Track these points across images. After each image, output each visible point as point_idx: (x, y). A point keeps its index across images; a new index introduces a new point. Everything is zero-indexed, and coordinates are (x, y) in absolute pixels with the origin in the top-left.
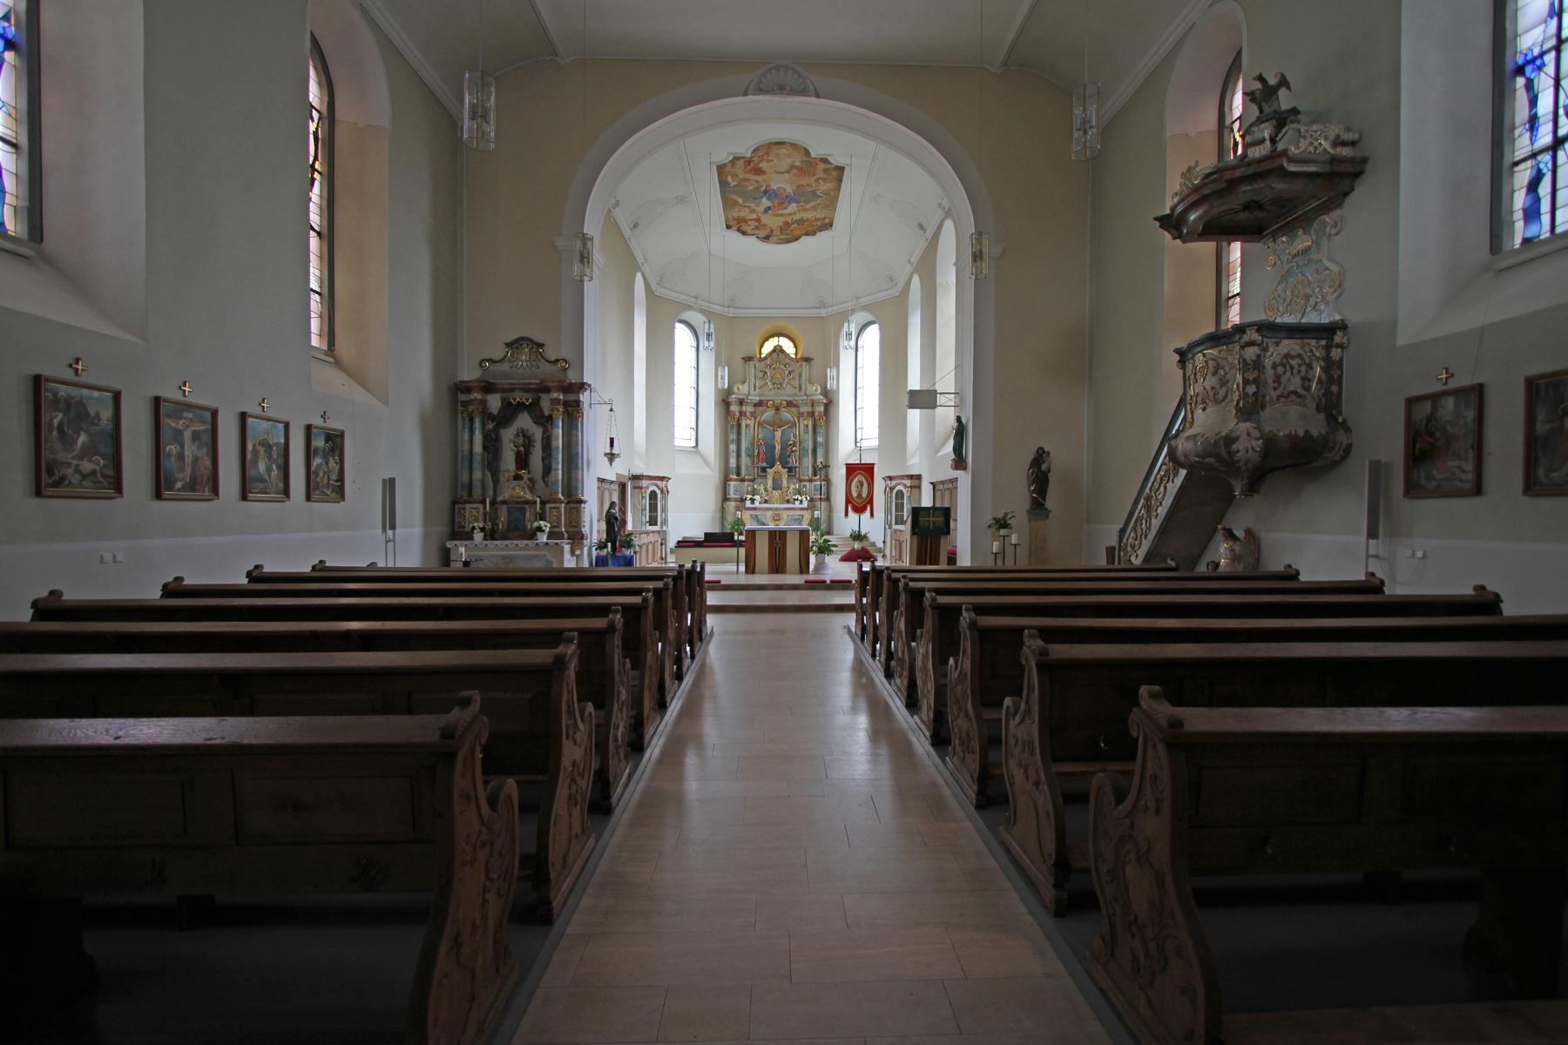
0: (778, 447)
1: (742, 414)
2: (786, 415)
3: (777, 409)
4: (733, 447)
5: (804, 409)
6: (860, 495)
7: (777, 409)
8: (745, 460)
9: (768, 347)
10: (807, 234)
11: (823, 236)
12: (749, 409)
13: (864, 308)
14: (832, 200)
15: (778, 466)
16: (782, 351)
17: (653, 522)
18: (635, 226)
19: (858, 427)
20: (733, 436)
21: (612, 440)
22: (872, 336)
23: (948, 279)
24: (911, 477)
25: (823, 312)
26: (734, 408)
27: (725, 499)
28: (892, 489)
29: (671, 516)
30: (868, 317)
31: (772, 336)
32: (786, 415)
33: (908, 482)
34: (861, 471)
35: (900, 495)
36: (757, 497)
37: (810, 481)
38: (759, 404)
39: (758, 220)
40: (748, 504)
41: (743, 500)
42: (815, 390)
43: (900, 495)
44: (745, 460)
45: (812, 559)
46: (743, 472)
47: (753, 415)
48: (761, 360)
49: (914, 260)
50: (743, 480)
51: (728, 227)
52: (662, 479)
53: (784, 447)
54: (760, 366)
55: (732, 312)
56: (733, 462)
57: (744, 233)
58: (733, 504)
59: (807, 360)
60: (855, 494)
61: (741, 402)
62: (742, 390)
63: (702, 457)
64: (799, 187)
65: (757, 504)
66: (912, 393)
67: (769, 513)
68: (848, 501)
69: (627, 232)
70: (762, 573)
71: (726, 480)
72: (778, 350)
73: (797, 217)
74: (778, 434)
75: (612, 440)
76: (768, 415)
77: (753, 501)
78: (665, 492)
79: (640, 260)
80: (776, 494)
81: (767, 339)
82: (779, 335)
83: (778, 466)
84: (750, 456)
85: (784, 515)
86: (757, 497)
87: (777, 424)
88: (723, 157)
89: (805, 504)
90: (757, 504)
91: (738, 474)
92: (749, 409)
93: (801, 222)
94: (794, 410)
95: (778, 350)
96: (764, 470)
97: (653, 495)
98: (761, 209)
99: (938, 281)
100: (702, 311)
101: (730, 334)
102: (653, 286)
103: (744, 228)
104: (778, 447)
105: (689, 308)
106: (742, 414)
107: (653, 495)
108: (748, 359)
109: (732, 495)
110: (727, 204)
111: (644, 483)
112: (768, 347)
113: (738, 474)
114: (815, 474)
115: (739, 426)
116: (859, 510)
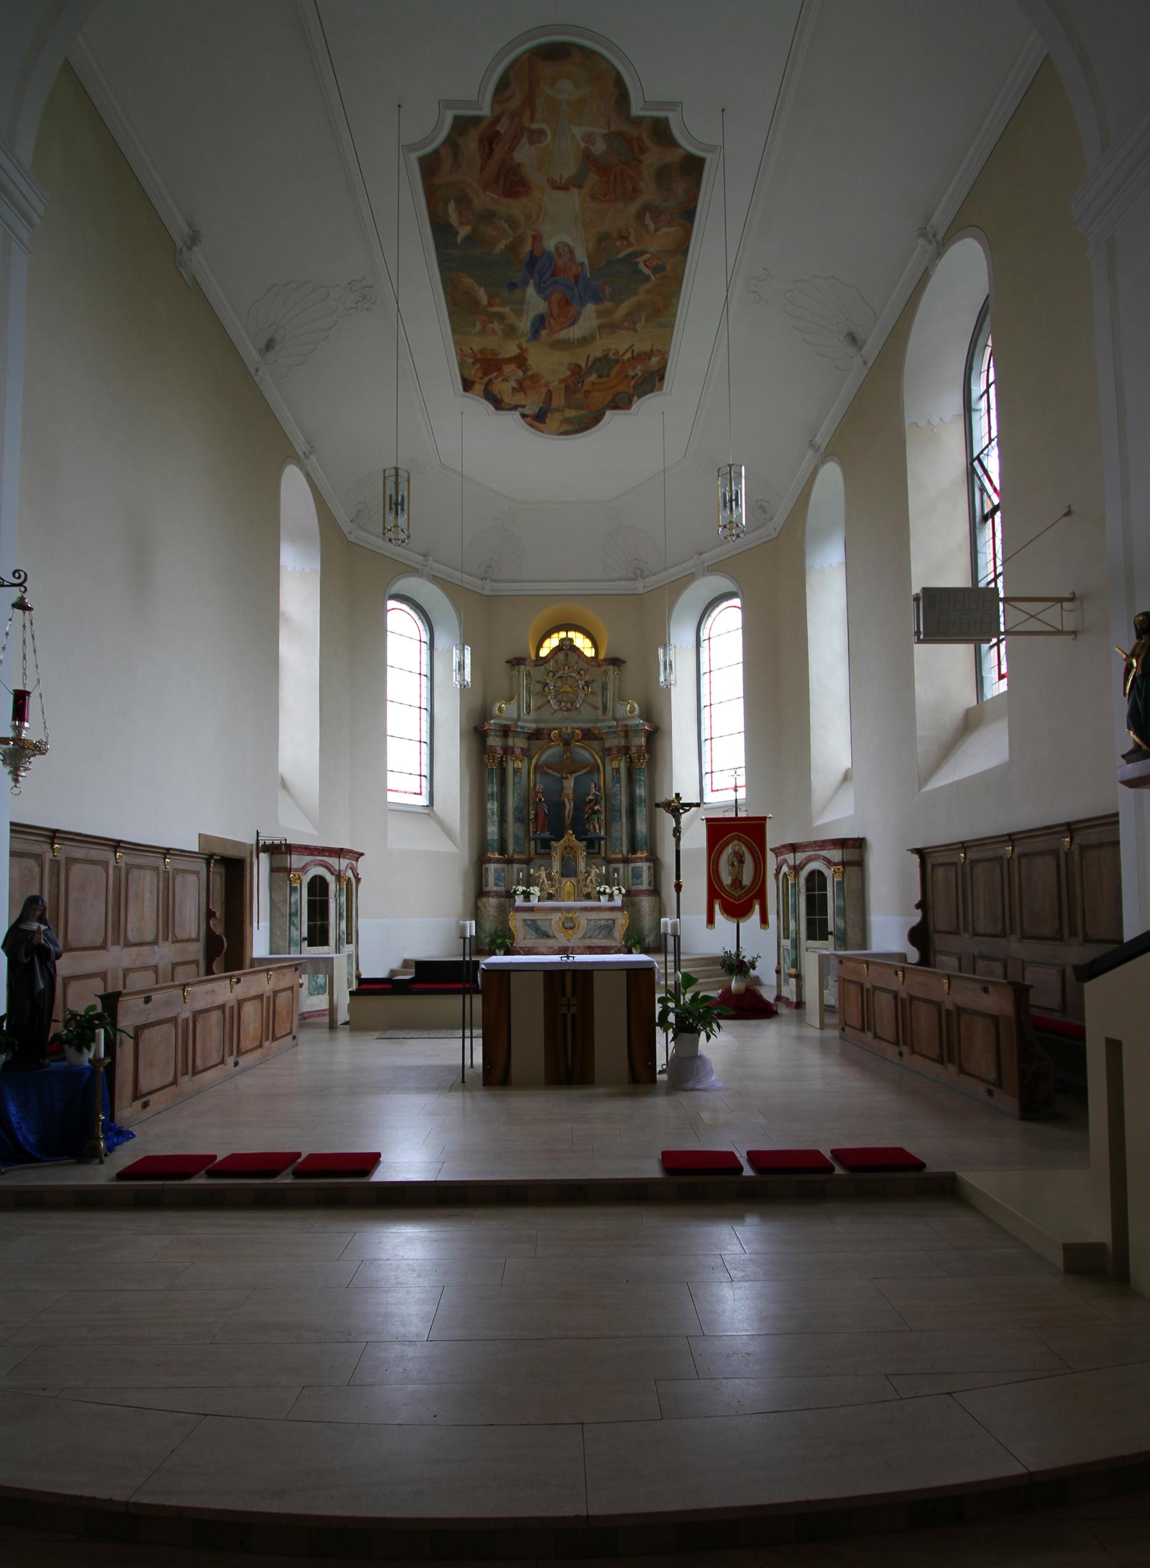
0: (569, 806)
1: (507, 750)
2: (583, 753)
3: (567, 743)
4: (493, 806)
5: (612, 742)
6: (737, 882)
7: (567, 743)
8: (512, 827)
9: (552, 642)
10: (616, 406)
11: (647, 406)
12: (518, 743)
13: (713, 569)
14: (662, 309)
15: (570, 837)
16: (575, 650)
17: (318, 936)
18: (270, 345)
19: (711, 759)
20: (493, 788)
21: (20, 699)
22: (727, 625)
23: (556, 958)
24: (842, 843)
25: (640, 587)
26: (494, 741)
27: (480, 892)
28: (796, 869)
29: (365, 925)
30: (722, 583)
31: (557, 629)
32: (583, 753)
33: (836, 855)
34: (736, 834)
35: (816, 881)
36: (535, 890)
37: (626, 861)
38: (536, 735)
39: (520, 361)
40: (519, 901)
41: (510, 895)
42: (630, 711)
43: (816, 881)
44: (512, 827)
45: (664, 1045)
46: (511, 848)
47: (527, 753)
48: (540, 661)
49: (822, 439)
50: (510, 861)
51: (468, 385)
52: (339, 853)
53: (581, 804)
54: (538, 673)
55: (488, 589)
56: (493, 830)
57: (498, 404)
58: (493, 901)
59: (616, 662)
60: (727, 880)
61: (505, 732)
62: (504, 711)
63: (440, 822)
64: (603, 238)
65: (534, 901)
66: (932, 597)
67: (556, 917)
68: (714, 892)
69: (250, 353)
70: (528, 1085)
71: (481, 861)
72: (567, 647)
73: (596, 350)
74: (569, 784)
75: (20, 699)
76: (551, 753)
77: (527, 896)
78: (350, 887)
79: (300, 448)
80: (568, 884)
81: (548, 635)
82: (568, 628)
83: (570, 837)
84: (522, 819)
85: (583, 919)
86: (535, 890)
87: (568, 766)
88: (429, 127)
89: (618, 901)
90: (534, 901)
91: (503, 850)
92: (518, 743)
93: (604, 364)
94: (595, 744)
95: (567, 647)
96: (546, 844)
97: (318, 887)
98: (525, 325)
99: (807, 565)
100: (435, 579)
101: (480, 611)
102: (343, 519)
103: (503, 388)
104: (569, 806)
105: (412, 571)
106: (507, 750)
107: (318, 887)
108: (516, 662)
109: (491, 886)
110: (462, 309)
111: (296, 861)
112: (552, 642)
113: (503, 850)
114: (633, 848)
115: (503, 771)
116: (737, 911)
